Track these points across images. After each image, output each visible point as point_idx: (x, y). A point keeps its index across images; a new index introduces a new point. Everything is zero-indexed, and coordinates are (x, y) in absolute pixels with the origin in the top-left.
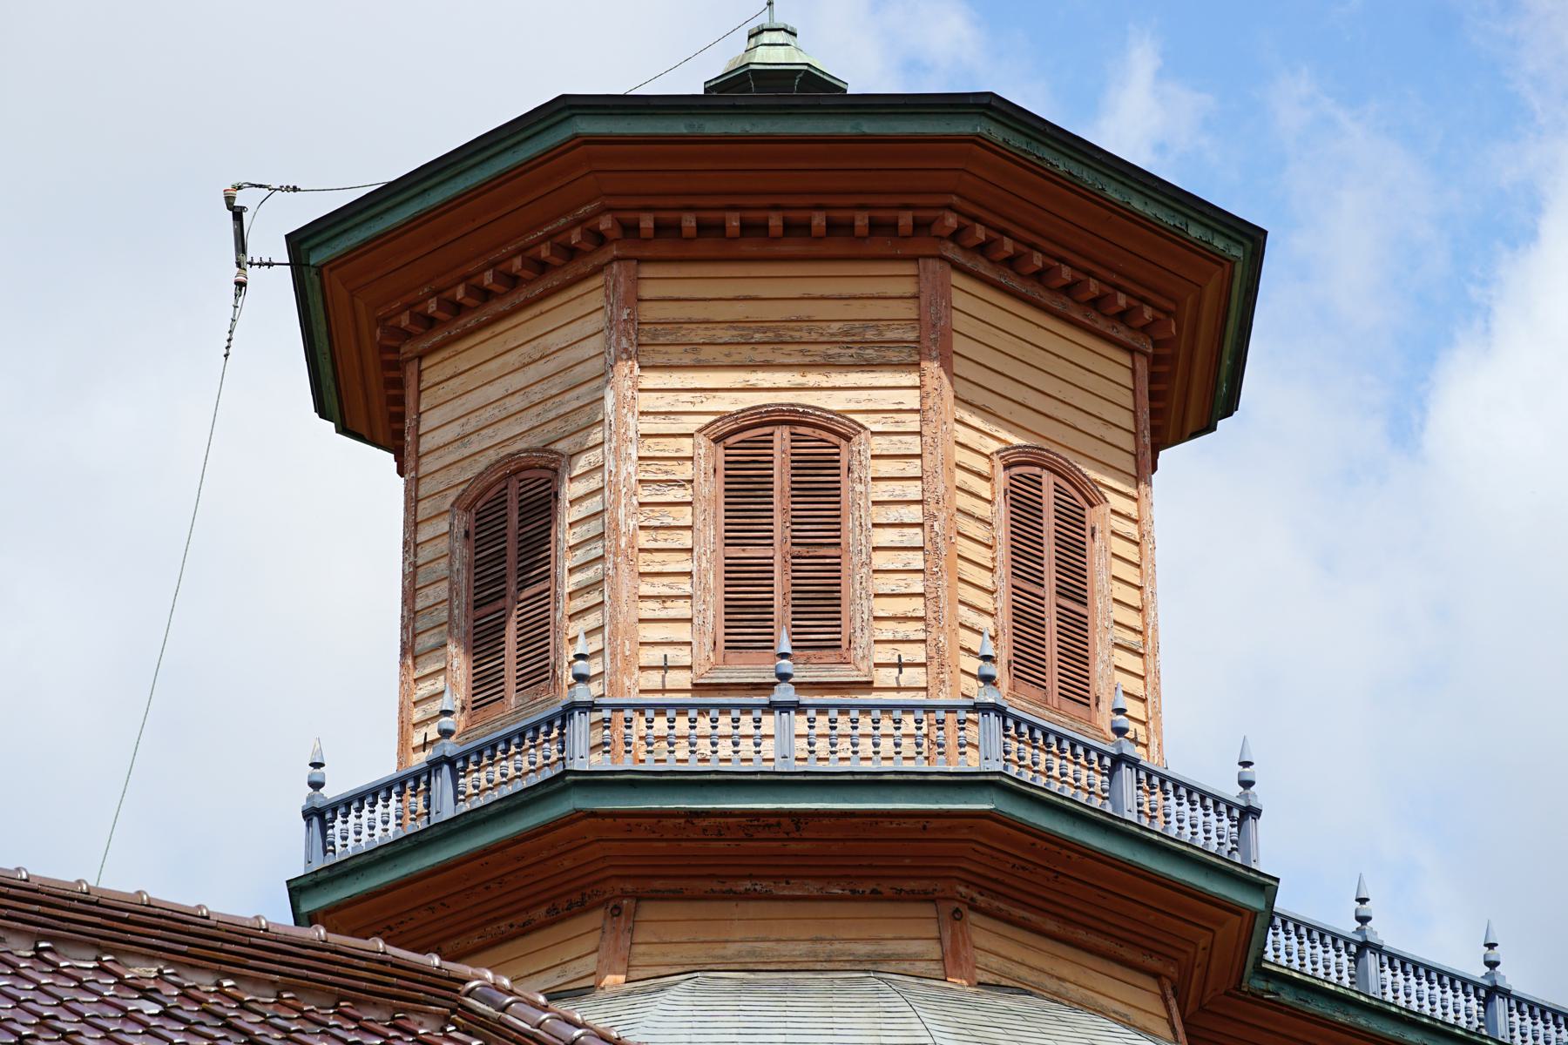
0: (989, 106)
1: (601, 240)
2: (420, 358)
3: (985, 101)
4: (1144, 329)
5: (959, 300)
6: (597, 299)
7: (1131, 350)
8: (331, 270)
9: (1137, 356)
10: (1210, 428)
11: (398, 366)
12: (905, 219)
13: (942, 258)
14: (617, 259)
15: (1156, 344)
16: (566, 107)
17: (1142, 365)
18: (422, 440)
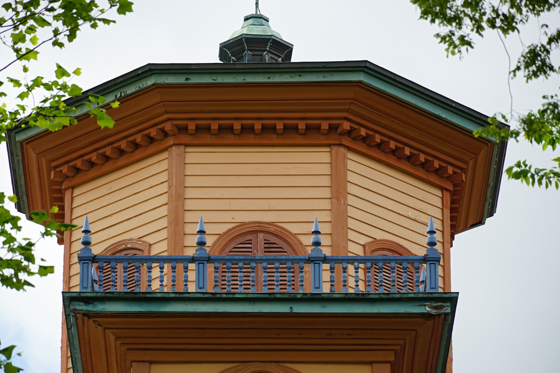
0: (150, 70)
1: (166, 134)
2: (73, 188)
3: (147, 68)
4: (449, 178)
5: (351, 165)
6: (164, 165)
7: (442, 189)
8: (27, 143)
9: (445, 192)
10: (481, 222)
11: (61, 191)
12: (325, 125)
13: (340, 145)
14: (174, 145)
15: (455, 185)
16: (151, 70)
17: (447, 195)
18: (74, 210)
